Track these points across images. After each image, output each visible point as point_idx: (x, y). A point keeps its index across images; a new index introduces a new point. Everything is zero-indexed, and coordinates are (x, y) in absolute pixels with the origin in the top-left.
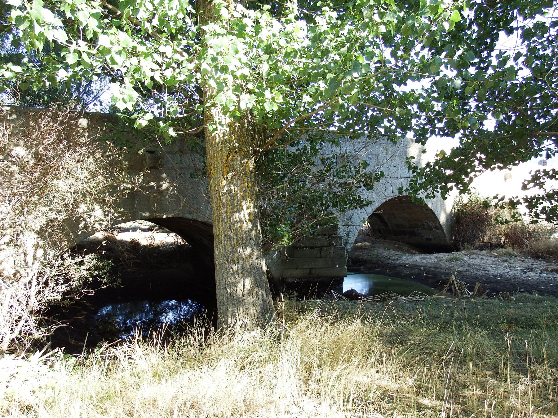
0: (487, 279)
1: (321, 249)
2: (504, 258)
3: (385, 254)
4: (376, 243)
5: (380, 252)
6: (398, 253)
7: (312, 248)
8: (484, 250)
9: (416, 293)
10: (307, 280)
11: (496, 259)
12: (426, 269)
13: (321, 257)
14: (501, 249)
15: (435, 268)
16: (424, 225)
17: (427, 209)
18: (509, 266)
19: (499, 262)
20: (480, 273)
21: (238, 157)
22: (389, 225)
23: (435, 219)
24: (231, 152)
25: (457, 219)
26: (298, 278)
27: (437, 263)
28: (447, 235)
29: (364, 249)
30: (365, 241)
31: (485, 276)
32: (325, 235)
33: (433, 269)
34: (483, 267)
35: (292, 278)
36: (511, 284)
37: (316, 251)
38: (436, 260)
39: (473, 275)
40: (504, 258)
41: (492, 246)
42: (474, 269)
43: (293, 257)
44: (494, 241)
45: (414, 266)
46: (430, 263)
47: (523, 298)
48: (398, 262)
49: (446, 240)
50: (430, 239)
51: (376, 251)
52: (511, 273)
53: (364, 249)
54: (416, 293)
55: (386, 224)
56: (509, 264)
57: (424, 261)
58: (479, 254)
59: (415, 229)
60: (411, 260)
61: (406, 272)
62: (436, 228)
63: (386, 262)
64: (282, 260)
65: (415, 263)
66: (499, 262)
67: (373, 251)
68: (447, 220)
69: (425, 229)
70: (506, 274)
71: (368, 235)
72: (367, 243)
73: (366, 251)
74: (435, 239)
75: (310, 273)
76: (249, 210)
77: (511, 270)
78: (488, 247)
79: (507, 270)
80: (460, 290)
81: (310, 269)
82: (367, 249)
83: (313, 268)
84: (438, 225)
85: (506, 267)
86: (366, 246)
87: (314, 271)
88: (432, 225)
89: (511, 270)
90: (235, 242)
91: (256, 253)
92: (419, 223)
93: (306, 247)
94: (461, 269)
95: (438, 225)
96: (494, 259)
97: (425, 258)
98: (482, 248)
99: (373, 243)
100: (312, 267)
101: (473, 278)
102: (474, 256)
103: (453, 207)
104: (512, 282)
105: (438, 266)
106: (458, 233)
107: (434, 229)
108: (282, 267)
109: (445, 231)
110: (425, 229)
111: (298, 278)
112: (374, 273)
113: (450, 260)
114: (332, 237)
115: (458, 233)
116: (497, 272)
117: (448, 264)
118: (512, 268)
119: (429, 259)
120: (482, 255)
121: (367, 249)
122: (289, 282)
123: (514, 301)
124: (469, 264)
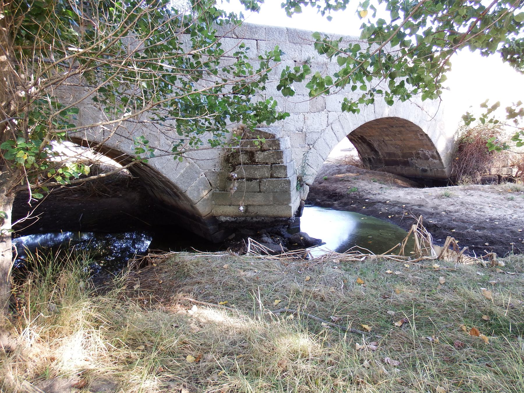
0: (481, 223)
1: (260, 182)
2: (510, 196)
3: (366, 187)
5: (362, 184)
6: (383, 186)
7: (249, 180)
8: (486, 184)
9: (356, 249)
10: (244, 219)
11: (499, 196)
12: (407, 207)
13: (260, 192)
14: (508, 184)
15: (420, 206)
16: (418, 154)
17: (422, 135)
18: (514, 206)
19: (502, 200)
20: (474, 214)
22: (380, 153)
23: (432, 146)
25: (460, 147)
26: (232, 217)
27: (423, 200)
28: (445, 166)
29: (346, 181)
30: (349, 171)
31: (479, 219)
32: (267, 164)
33: (417, 208)
34: (479, 207)
35: (226, 216)
36: (512, 232)
37: (254, 183)
38: (423, 197)
39: (464, 218)
40: (510, 196)
41: (499, 179)
42: (467, 208)
43: (227, 191)
44: (504, 173)
45: (395, 204)
46: (415, 200)
47: (518, 264)
48: (380, 197)
49: (443, 172)
50: (425, 171)
51: (358, 183)
52: (515, 216)
53: (346, 181)
54: (356, 249)
55: (376, 152)
56: (515, 203)
57: (409, 197)
58: (480, 190)
59: (409, 159)
60: (393, 196)
61: (384, 209)
62: (433, 157)
63: (365, 197)
64: (213, 194)
65: (397, 200)
66: (502, 200)
67: (355, 183)
68: (447, 148)
69: (420, 158)
70: (508, 217)
71: (357, 166)
73: (347, 184)
74: (431, 170)
77: (515, 212)
78: (494, 180)
79: (510, 212)
80: (422, 246)
82: (348, 181)
83: (250, 205)
84: (435, 153)
85: (510, 207)
87: (251, 209)
88: (428, 153)
89: (515, 212)
92: (414, 152)
94: (451, 208)
95: (435, 153)
96: (496, 197)
97: (411, 193)
98: (484, 182)
100: (249, 203)
101: (463, 221)
102: (472, 192)
103: (457, 132)
104: (513, 228)
105: (423, 204)
106: (459, 163)
107: (431, 159)
108: (213, 202)
109: (443, 161)
110: (420, 158)
111: (232, 217)
112: (348, 210)
113: (440, 197)
114: (276, 167)
115: (459, 163)
116: (495, 213)
117: (436, 201)
118: (518, 209)
119: (415, 194)
120: (484, 191)
121: (348, 181)
122: (222, 221)
123: (502, 268)
124: (462, 203)
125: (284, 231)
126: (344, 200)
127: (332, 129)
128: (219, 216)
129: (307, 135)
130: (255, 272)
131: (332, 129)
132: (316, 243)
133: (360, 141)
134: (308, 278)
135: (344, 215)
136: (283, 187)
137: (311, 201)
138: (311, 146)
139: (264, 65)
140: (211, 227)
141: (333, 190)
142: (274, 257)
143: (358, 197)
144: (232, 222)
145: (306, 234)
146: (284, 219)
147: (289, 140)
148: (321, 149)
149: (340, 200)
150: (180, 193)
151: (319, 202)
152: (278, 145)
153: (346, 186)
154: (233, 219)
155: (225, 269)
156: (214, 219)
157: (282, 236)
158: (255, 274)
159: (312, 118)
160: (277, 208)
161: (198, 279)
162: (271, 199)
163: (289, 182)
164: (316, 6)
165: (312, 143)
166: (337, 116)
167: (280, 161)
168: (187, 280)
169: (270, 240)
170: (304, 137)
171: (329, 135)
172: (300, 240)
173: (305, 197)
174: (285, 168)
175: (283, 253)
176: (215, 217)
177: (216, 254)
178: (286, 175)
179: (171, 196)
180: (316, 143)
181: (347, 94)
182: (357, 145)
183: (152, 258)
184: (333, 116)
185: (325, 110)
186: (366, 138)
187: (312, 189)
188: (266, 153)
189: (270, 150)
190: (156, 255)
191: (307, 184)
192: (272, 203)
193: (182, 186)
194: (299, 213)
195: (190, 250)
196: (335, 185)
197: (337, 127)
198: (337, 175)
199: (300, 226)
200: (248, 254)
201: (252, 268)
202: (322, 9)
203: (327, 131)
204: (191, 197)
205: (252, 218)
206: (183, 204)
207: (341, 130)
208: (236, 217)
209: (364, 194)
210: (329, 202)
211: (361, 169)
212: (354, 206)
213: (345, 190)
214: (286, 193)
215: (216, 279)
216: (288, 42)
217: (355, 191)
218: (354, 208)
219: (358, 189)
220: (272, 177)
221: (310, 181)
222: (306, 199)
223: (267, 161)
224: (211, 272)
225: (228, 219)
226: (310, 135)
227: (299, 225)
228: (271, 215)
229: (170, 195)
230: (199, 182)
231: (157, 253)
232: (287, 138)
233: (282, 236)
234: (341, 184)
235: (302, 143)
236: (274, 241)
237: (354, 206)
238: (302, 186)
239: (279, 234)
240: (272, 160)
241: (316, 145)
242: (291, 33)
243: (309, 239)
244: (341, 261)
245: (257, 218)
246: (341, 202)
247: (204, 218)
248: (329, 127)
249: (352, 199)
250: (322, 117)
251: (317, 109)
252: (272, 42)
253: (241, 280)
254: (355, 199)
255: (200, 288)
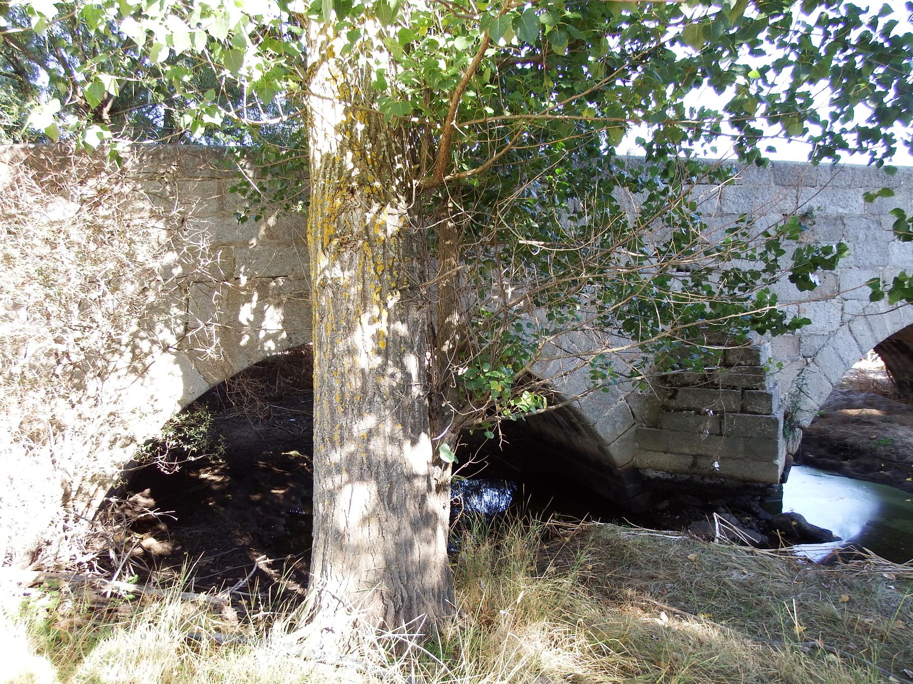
4: (897, 413)
5: (901, 433)
10: (687, 477)
21: (357, 200)
24: (340, 189)
26: (668, 472)
29: (865, 423)
30: (870, 405)
32: (734, 388)
35: (656, 469)
43: (661, 428)
51: (891, 430)
53: (865, 423)
64: (637, 431)
67: (884, 430)
71: (885, 395)
72: (875, 412)
73: (867, 428)
75: (694, 464)
76: (377, 325)
81: (695, 457)
83: (701, 456)
86: (870, 416)
90: (338, 399)
91: (388, 427)
93: (689, 409)
99: (889, 411)
100: (700, 452)
108: (637, 444)
111: (668, 472)
112: (873, 480)
114: (750, 394)
122: (649, 478)
125: (756, 507)
126: (864, 461)
127: (851, 331)
128: (645, 469)
129: (803, 340)
130: (744, 574)
131: (851, 331)
132: (818, 536)
133: (894, 349)
134: (845, 598)
135: (858, 487)
136: (764, 430)
137: (801, 459)
138: (809, 360)
139: (773, 245)
140: (630, 486)
141: (839, 439)
142: (765, 551)
143: (894, 457)
144: (667, 480)
145: (800, 516)
146: (761, 485)
147: (770, 348)
148: (828, 365)
149: (854, 458)
150: (583, 426)
151: (810, 458)
152: (757, 357)
153: (867, 433)
154: (669, 477)
155: (691, 561)
156: (635, 472)
157: (755, 515)
158: (745, 577)
159: (812, 311)
160: (751, 465)
161: (651, 572)
162: (741, 448)
163: (776, 422)
164: (868, 152)
165: (811, 354)
166: (861, 308)
167: (759, 384)
168: (631, 570)
169: (734, 519)
170: (796, 343)
171: (843, 340)
172: (790, 526)
173: (795, 447)
174: (769, 397)
175: (782, 547)
176: (637, 469)
177: (667, 534)
178: (771, 410)
179: (561, 427)
180: (819, 355)
181: (881, 268)
182: (886, 356)
183: (558, 527)
184: (852, 307)
185: (838, 297)
186: (908, 344)
187: (808, 437)
188: (732, 370)
189: (740, 364)
190: (564, 524)
191: (801, 428)
192: (741, 456)
193: (589, 416)
194: (784, 479)
195: (621, 523)
196: (841, 430)
197: (859, 326)
198: (844, 411)
199: (784, 500)
200: (717, 540)
201: (737, 565)
202: (878, 156)
203: (840, 334)
204: (601, 433)
205: (703, 478)
206: (583, 443)
207: (868, 333)
208: (674, 472)
209: (908, 452)
210: (833, 461)
211: (896, 404)
212: (887, 473)
213: (866, 441)
214: (771, 440)
215: (683, 575)
216: (773, 184)
217: (886, 445)
218: (888, 477)
219: (893, 441)
220: (743, 410)
221: (806, 420)
222: (795, 451)
223: (735, 384)
224: (670, 564)
225: (660, 474)
226: (809, 340)
227: (781, 498)
228: (739, 476)
229: (561, 427)
230: (616, 410)
231: (567, 520)
232: (768, 345)
233: (755, 515)
234: (855, 429)
235: (793, 354)
236: (741, 522)
237: (887, 473)
238: (792, 429)
239: (750, 512)
240: (745, 383)
241: (818, 358)
242: (779, 169)
243: (809, 528)
244: (898, 577)
245: (711, 479)
246: (858, 464)
247: (619, 469)
248: (845, 328)
249: (882, 460)
250: (831, 310)
251: (822, 294)
252: (744, 186)
253: (725, 584)
254: (888, 460)
255: (657, 585)
